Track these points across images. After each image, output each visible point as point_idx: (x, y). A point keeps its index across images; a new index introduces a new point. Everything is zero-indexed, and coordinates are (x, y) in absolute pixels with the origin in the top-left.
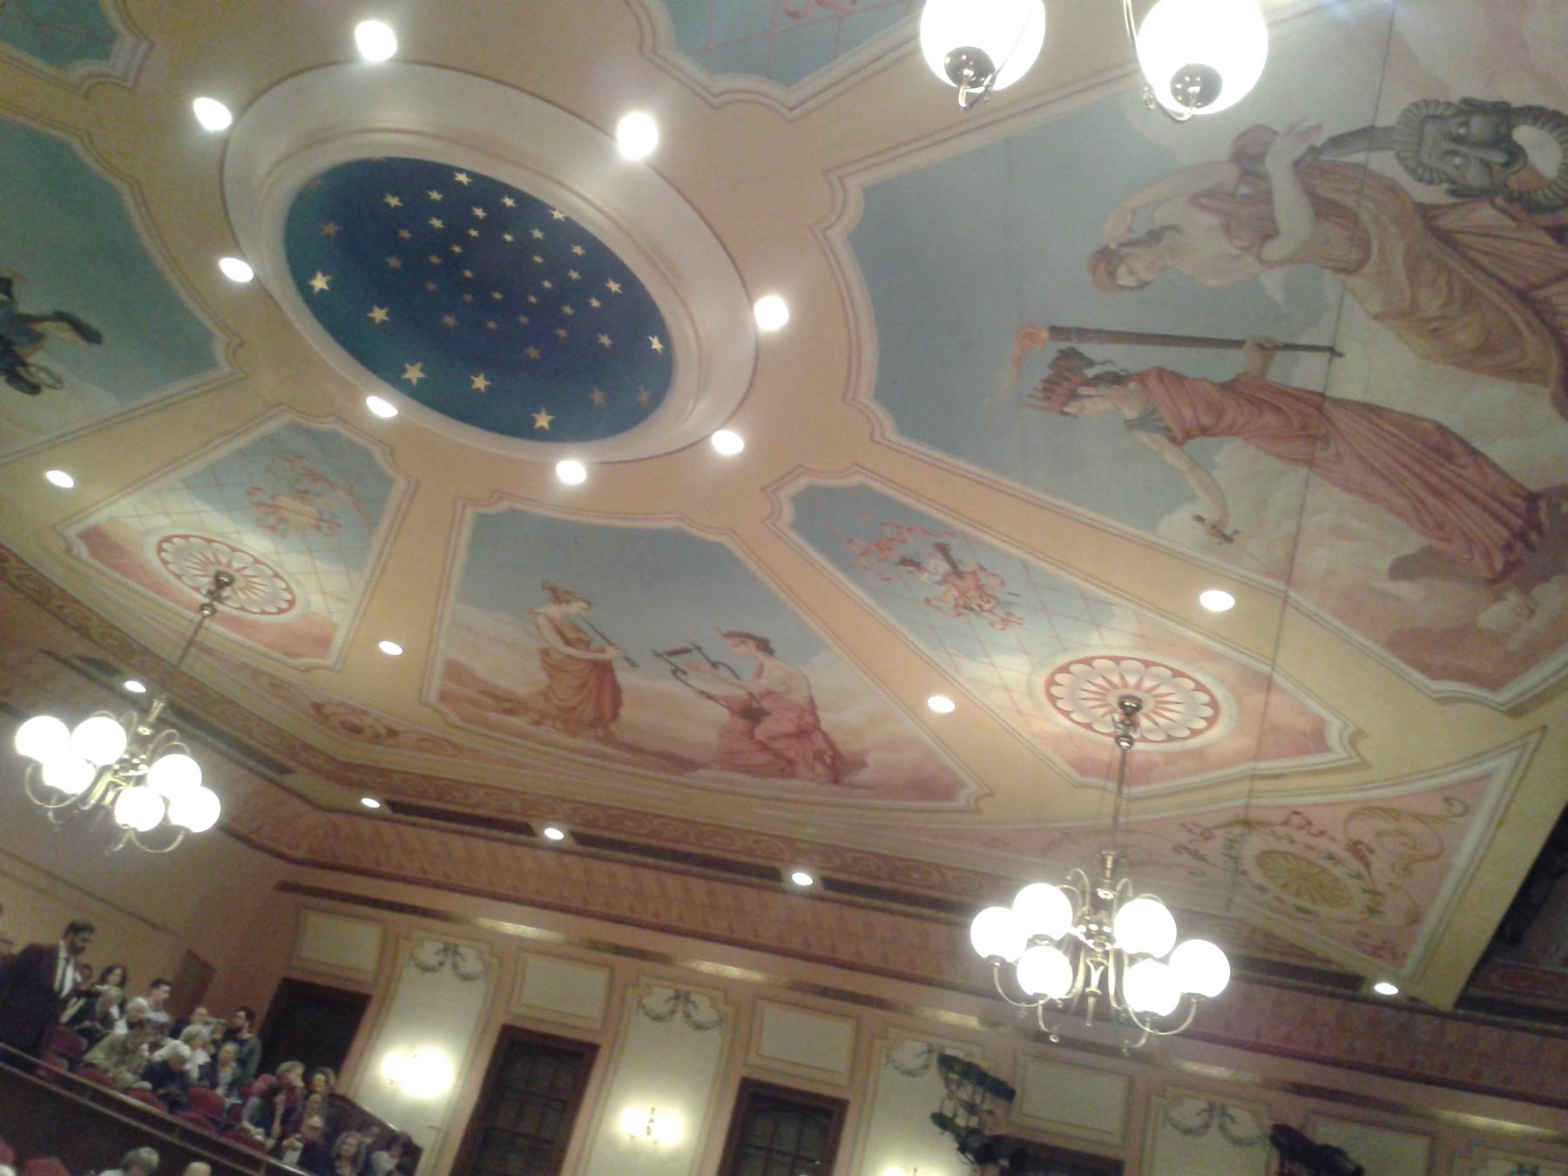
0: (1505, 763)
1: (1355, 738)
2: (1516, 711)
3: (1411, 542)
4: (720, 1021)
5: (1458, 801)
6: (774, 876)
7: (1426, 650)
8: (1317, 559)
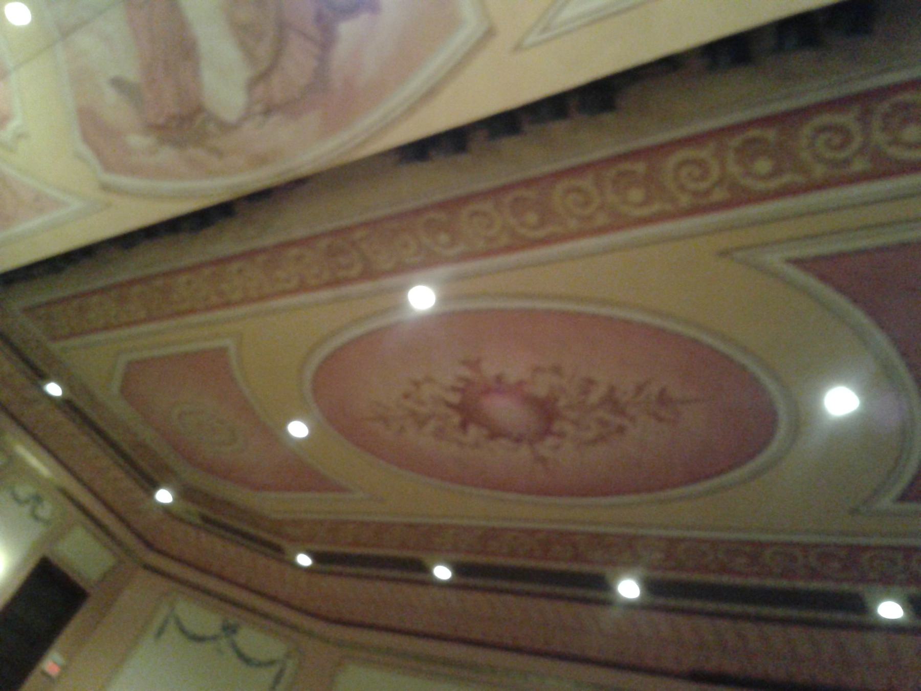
0: (76, 204)
1: (20, 136)
2: (106, 188)
3: (132, 73)
4: (47, 523)
5: (40, 203)
6: (598, 586)
7: (93, 128)
8: (84, 41)
